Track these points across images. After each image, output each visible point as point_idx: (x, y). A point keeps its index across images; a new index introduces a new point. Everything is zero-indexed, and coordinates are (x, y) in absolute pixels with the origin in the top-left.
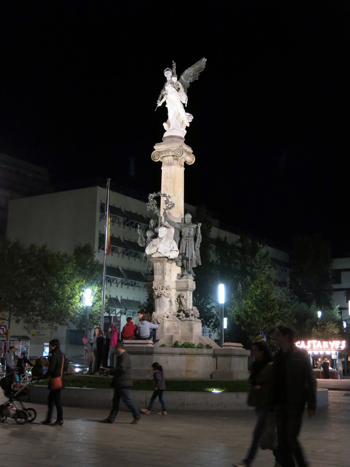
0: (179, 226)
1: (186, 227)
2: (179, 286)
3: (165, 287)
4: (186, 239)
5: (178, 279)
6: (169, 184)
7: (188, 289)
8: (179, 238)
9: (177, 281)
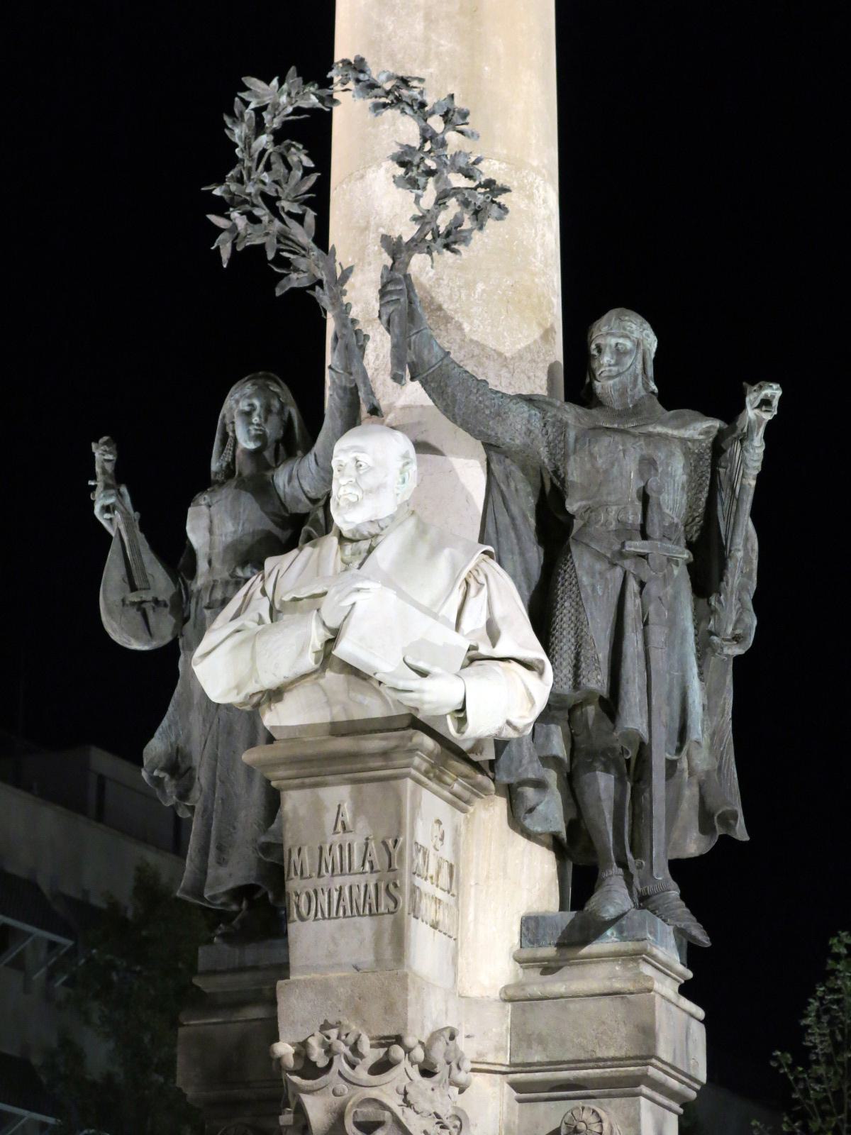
0: (537, 424)
1: (606, 440)
2: (541, 1041)
3: (410, 1041)
4: (622, 555)
5: (535, 974)
6: (419, 27)
7: (652, 1071)
8: (535, 555)
9: (520, 985)
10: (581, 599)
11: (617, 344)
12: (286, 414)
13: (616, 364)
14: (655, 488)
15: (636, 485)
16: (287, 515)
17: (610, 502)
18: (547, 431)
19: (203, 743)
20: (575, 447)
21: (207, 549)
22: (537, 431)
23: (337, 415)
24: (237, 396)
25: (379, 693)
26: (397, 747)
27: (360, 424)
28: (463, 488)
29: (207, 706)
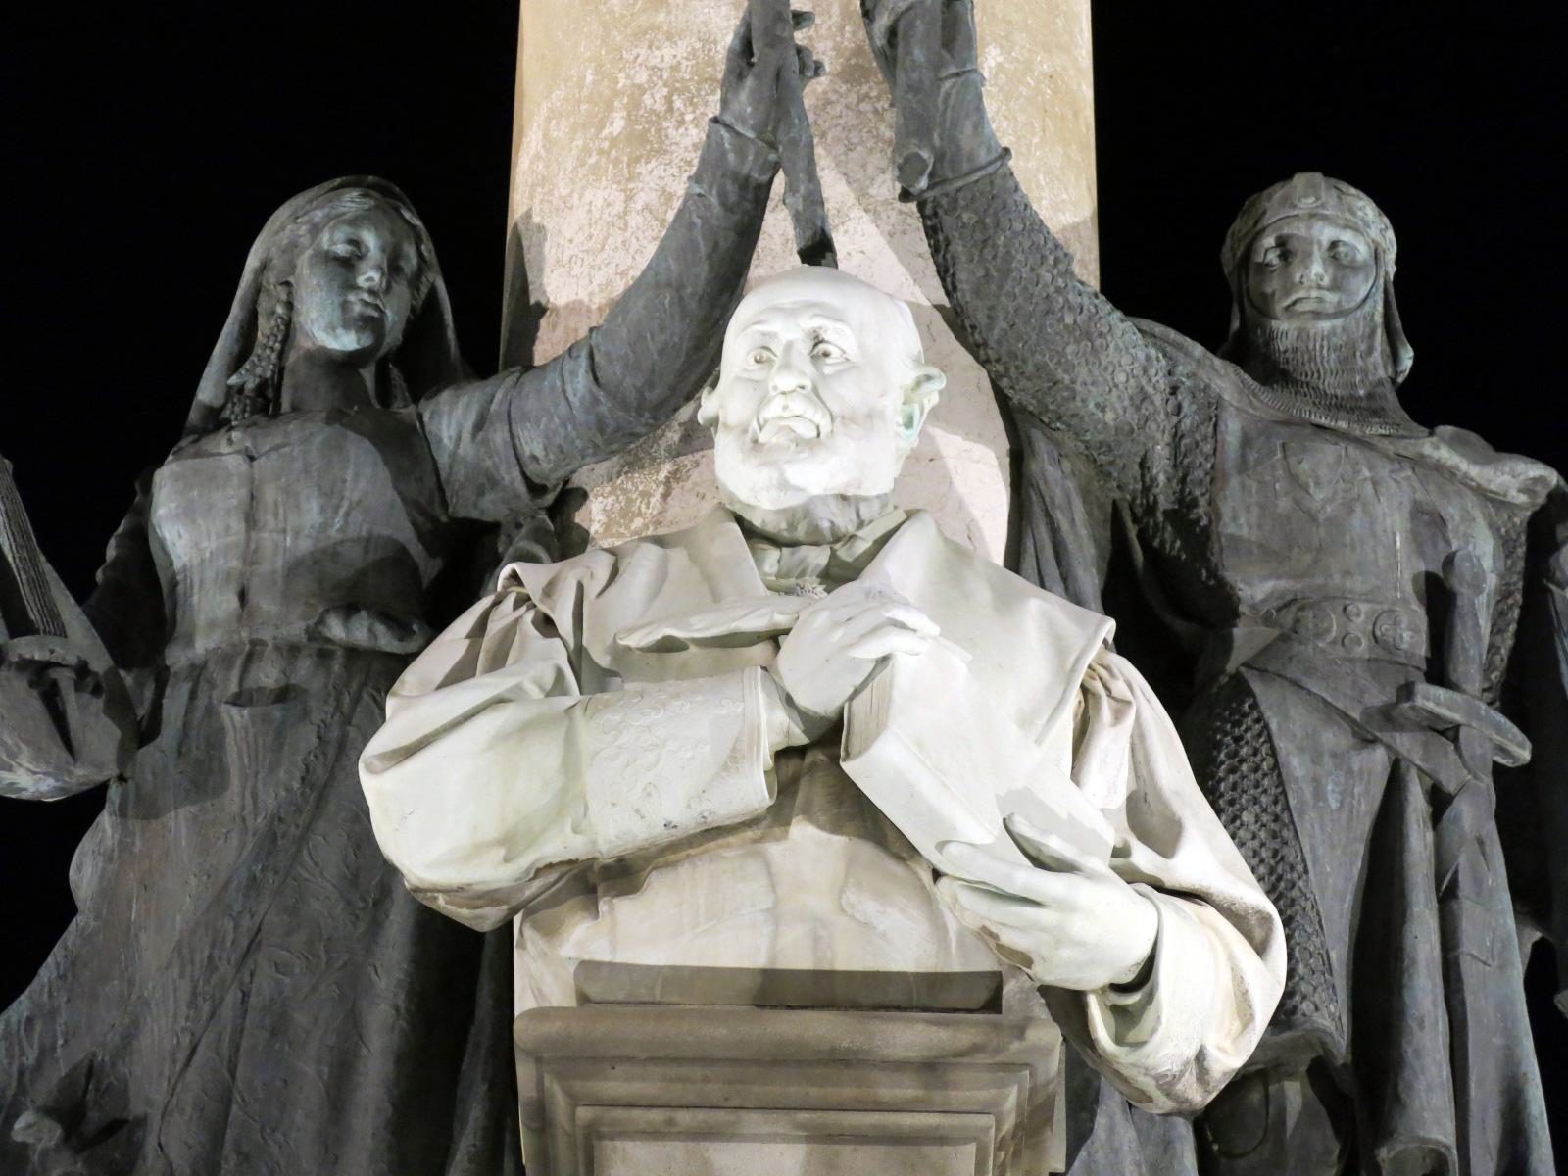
10: (1287, 808)
11: (1334, 245)
12: (424, 290)
13: (1335, 287)
14: (1468, 578)
15: (1408, 568)
16: (444, 519)
17: (1352, 592)
18: (1179, 407)
19: (182, 1057)
20: (1243, 457)
21: (235, 564)
22: (1158, 400)
23: (703, 249)
24: (319, 215)
25: (929, 901)
26: (974, 1049)
27: (820, 264)
28: (961, 505)
29: (210, 957)
